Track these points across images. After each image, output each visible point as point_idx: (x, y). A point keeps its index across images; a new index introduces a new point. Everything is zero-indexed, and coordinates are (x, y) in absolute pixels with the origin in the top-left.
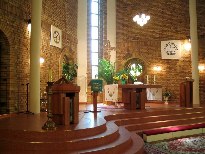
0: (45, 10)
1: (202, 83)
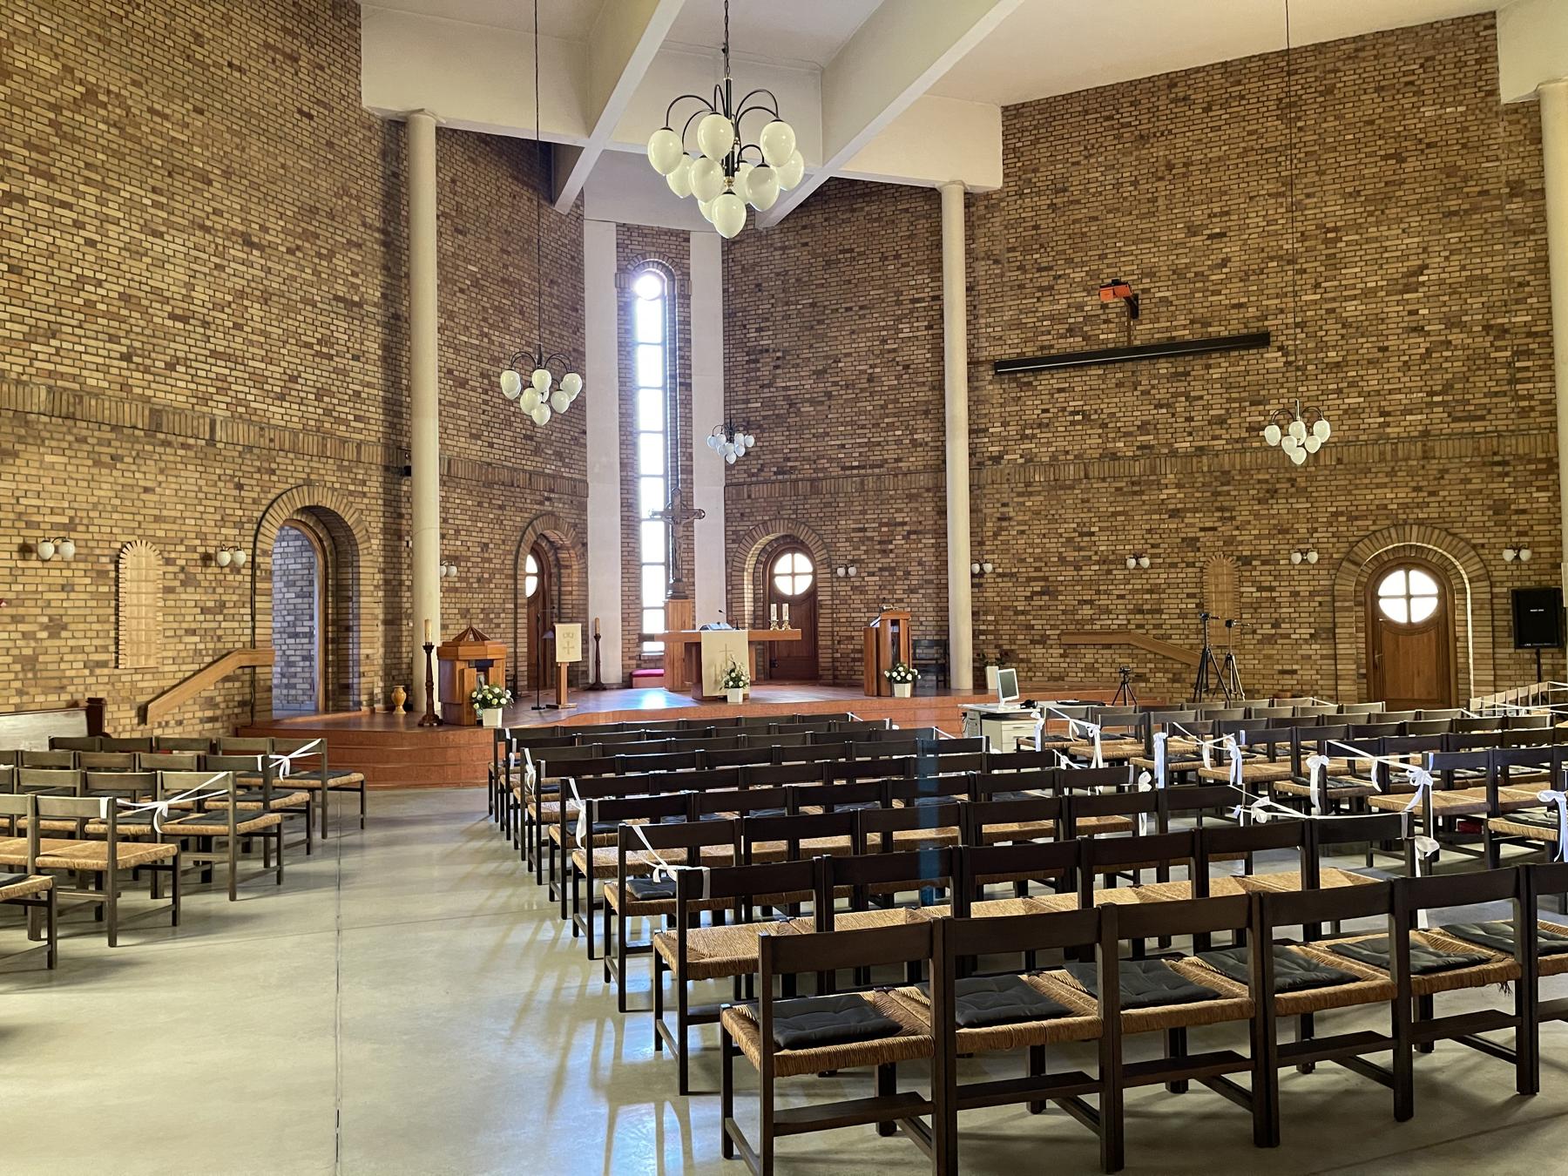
0: (459, 422)
1: (992, 618)
